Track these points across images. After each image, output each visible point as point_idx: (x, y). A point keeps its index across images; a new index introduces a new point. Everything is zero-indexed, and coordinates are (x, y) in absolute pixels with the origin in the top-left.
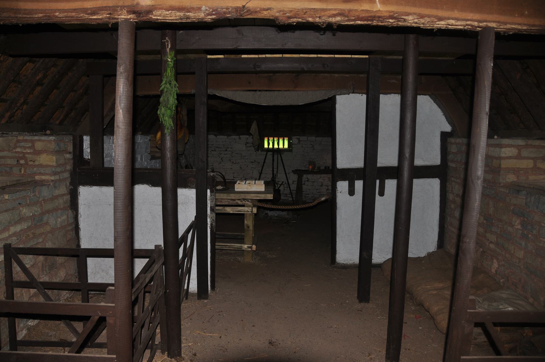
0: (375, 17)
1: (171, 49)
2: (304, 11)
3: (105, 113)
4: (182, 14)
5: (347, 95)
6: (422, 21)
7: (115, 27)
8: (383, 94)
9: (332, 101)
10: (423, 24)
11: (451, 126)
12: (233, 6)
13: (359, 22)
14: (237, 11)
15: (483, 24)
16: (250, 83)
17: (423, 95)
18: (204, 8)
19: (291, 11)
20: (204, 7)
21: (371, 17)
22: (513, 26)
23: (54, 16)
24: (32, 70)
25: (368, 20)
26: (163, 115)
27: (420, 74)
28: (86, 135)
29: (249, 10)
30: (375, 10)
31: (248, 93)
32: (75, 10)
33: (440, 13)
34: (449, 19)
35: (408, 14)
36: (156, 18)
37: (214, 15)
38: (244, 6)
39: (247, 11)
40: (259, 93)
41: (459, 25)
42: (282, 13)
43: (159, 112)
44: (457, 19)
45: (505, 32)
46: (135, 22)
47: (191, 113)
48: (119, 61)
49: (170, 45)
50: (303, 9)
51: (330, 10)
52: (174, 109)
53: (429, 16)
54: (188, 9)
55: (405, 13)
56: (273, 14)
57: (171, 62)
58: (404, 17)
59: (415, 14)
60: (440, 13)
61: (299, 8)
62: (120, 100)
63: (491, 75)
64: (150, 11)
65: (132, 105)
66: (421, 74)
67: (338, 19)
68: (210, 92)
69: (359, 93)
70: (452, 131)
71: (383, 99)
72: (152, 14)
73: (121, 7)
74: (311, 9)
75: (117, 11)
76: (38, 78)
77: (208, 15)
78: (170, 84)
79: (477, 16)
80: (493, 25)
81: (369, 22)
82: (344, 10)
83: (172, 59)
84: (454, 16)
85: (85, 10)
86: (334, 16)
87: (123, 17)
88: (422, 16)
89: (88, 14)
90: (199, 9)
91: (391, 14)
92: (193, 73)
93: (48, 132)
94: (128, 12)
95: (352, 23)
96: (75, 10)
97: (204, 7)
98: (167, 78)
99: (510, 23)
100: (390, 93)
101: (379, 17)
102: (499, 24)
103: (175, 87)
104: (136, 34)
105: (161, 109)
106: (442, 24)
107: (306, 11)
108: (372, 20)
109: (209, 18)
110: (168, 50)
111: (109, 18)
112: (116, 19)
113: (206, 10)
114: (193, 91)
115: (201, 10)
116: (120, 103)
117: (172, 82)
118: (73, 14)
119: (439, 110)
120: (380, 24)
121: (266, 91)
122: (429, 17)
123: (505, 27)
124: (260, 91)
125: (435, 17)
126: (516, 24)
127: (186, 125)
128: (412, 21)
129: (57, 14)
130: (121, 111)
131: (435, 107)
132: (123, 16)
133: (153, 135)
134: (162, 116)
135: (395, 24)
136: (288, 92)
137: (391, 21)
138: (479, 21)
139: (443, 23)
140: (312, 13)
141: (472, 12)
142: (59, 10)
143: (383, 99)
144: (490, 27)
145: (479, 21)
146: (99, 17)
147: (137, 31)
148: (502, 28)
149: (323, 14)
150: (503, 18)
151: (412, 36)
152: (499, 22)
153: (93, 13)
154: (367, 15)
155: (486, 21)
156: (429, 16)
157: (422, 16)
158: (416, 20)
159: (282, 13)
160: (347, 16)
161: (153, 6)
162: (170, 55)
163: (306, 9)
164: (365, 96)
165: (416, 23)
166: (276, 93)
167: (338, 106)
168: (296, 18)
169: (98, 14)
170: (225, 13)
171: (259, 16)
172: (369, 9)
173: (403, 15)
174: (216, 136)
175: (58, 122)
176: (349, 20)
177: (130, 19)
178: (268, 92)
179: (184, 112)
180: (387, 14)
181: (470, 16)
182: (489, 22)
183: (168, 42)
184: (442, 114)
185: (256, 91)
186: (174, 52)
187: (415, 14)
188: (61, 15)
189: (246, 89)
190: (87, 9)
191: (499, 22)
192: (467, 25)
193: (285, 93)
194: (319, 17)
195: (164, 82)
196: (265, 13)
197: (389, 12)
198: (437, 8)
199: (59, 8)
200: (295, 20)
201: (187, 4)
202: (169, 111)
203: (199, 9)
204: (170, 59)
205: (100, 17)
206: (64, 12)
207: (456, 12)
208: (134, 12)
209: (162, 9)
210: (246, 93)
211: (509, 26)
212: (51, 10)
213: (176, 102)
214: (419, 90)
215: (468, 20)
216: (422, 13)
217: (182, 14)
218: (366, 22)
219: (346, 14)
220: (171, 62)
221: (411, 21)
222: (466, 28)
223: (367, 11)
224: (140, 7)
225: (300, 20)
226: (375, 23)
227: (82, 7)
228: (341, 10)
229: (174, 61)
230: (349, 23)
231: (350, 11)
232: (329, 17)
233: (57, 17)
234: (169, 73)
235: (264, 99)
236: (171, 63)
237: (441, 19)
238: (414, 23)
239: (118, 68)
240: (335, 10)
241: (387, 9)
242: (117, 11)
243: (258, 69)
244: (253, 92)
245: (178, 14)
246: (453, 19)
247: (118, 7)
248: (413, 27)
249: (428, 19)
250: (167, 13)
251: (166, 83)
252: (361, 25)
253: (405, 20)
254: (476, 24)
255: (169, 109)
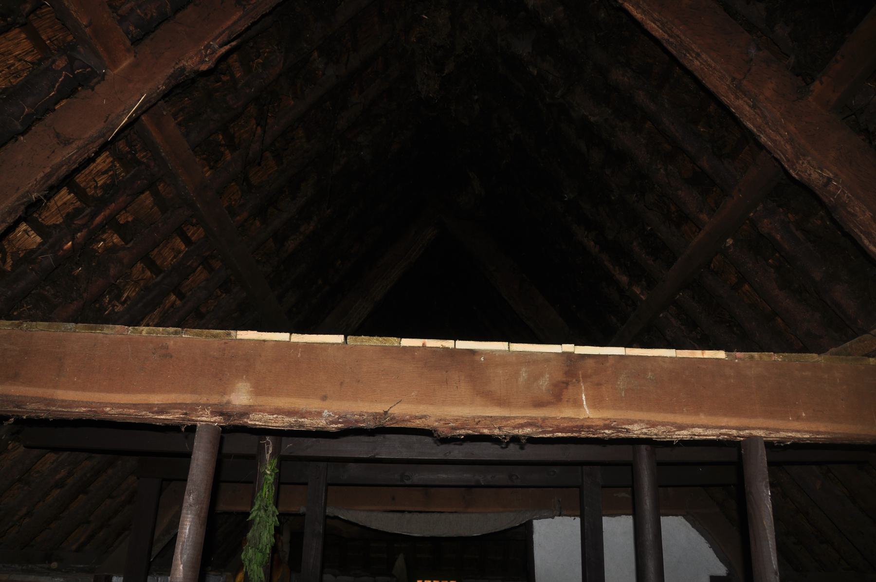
0: (582, 426)
1: (272, 455)
2: (477, 420)
3: (156, 537)
4: (292, 420)
5: (550, 519)
6: (654, 431)
7: (192, 429)
8: (608, 515)
9: (527, 529)
10: (656, 435)
11: (726, 565)
12: (370, 411)
13: (560, 434)
14: (375, 418)
15: (746, 433)
16: (393, 499)
17: (672, 515)
18: (326, 413)
19: (457, 420)
20: (326, 411)
21: (577, 426)
22: (790, 434)
23: (103, 411)
24: (52, 463)
25: (572, 432)
26: (250, 561)
27: (659, 485)
28: (118, 574)
29: (393, 419)
30: (582, 417)
31: (391, 515)
32: (134, 405)
33: (680, 419)
34: (693, 427)
35: (632, 422)
36: (253, 423)
37: (340, 423)
38: (386, 413)
39: (391, 419)
40: (408, 515)
41: (711, 434)
42: (442, 422)
43: (243, 557)
44: (706, 427)
45: (779, 442)
46: (221, 426)
47: (297, 539)
48: (189, 486)
49: (271, 449)
50: (474, 418)
51: (515, 418)
52: (268, 551)
53: (663, 424)
54: (302, 414)
55: (628, 420)
56: (430, 423)
57: (271, 475)
58: (627, 427)
59: (642, 421)
60: (680, 419)
61: (469, 416)
62: (182, 549)
63: (770, 510)
64: (245, 414)
65: (200, 557)
66: (660, 486)
67: (528, 430)
68: (330, 511)
69: (570, 516)
70: (728, 574)
71: (608, 523)
72: (248, 418)
73: (203, 405)
74: (486, 418)
75: (196, 410)
76: (58, 477)
77: (332, 422)
78: (266, 511)
79: (734, 422)
80: (761, 433)
81: (575, 435)
82: (536, 418)
83: (273, 470)
84: (700, 423)
85: (149, 407)
86: (522, 426)
87: (204, 419)
88: (653, 425)
89: (153, 413)
90: (319, 414)
91: (607, 422)
92: (306, 484)
93: (54, 565)
94: (212, 413)
95: (548, 435)
96: (135, 406)
97: (326, 411)
98: (262, 500)
99: (783, 430)
100: (620, 515)
101: (589, 427)
102: (767, 432)
103: (273, 516)
104: (222, 439)
105: (247, 552)
106: (684, 434)
107: (478, 420)
108: (580, 432)
109: (333, 427)
110: (268, 456)
111: (183, 419)
112: (193, 420)
113: (330, 415)
114: (302, 510)
115: (321, 416)
116: (181, 553)
117: (270, 508)
118: (132, 411)
119: (703, 540)
120: (591, 436)
121: (421, 512)
122: (663, 426)
123: (778, 435)
124: (410, 512)
125: (672, 424)
126: (793, 431)
127: (287, 559)
128: (639, 432)
129: (108, 409)
130: (181, 567)
131: (694, 534)
132: (205, 418)
133: (229, 574)
134: (247, 563)
135: (614, 436)
136: (455, 515)
137: (607, 431)
138: (738, 429)
139: (685, 432)
140: (488, 422)
141: (725, 415)
142: (111, 404)
143: (608, 523)
144: (756, 437)
145: (738, 429)
146: (168, 417)
147: (224, 435)
148: (774, 436)
149: (504, 423)
150: (772, 423)
151: (643, 447)
152: (767, 429)
153: (161, 412)
154: (570, 424)
155: (748, 428)
156: (663, 424)
157: (653, 425)
158: (645, 431)
159: (442, 422)
160: (541, 427)
161: (250, 406)
162: (271, 464)
163: (479, 417)
164: (578, 520)
165: (646, 434)
166: (436, 515)
167: (536, 537)
168: (464, 428)
169: (167, 413)
170: (357, 421)
171: (409, 425)
172: (573, 416)
173: (624, 424)
174: (335, 576)
175: (74, 547)
176: (544, 432)
177: (215, 422)
178: (422, 515)
179: (286, 537)
180: (601, 423)
181: (724, 421)
182: (753, 429)
183: (268, 443)
184: (707, 545)
185: (403, 512)
186: (276, 461)
187: (642, 421)
188: (113, 412)
189: (389, 508)
190: (153, 405)
191: (767, 429)
192: (721, 434)
193: (451, 516)
194: (499, 428)
195: (256, 507)
196: (418, 422)
197: (603, 419)
198: (673, 412)
199: (113, 401)
200: (463, 432)
201: (301, 407)
202: (260, 555)
203: (319, 414)
204: (269, 470)
205: (171, 417)
206: (119, 408)
207: (702, 416)
208: (221, 414)
209: (263, 411)
210: (386, 514)
211: (783, 434)
212: (100, 403)
213: (273, 540)
214: (664, 507)
215: (722, 428)
216: (653, 419)
217: (292, 420)
218: (569, 435)
219: (539, 424)
220: (271, 475)
221: (637, 430)
222: (720, 438)
223: (571, 419)
224: (231, 406)
225: (470, 432)
226: (583, 435)
227: (146, 402)
228: (531, 418)
229: (276, 474)
230: (544, 436)
231: (544, 419)
232: (514, 428)
233: (107, 413)
234: (266, 492)
235: (417, 525)
236: (270, 477)
237: (681, 427)
238: (642, 433)
239: (186, 497)
240: (523, 418)
241: (600, 416)
242: (196, 410)
243: (407, 482)
244: (399, 515)
245: (287, 419)
246: (699, 427)
247: (198, 405)
248: (642, 439)
249: (663, 429)
250: (271, 417)
251: (259, 509)
252: (563, 438)
253: (628, 431)
254: (734, 432)
255: (261, 551)
